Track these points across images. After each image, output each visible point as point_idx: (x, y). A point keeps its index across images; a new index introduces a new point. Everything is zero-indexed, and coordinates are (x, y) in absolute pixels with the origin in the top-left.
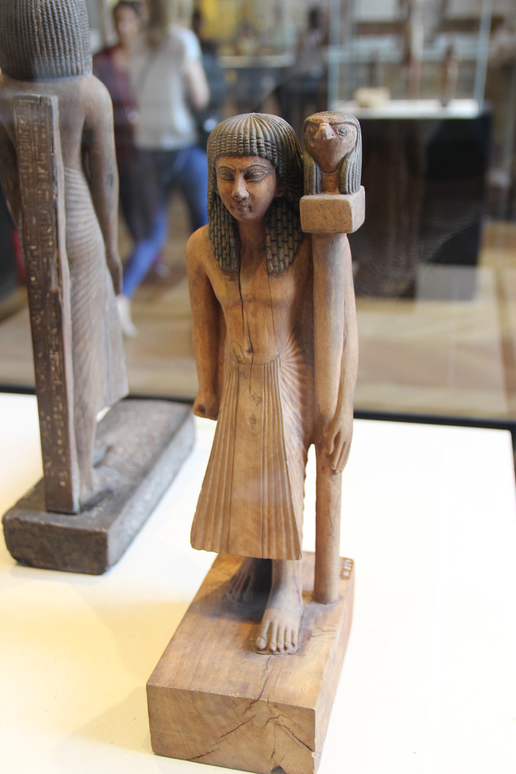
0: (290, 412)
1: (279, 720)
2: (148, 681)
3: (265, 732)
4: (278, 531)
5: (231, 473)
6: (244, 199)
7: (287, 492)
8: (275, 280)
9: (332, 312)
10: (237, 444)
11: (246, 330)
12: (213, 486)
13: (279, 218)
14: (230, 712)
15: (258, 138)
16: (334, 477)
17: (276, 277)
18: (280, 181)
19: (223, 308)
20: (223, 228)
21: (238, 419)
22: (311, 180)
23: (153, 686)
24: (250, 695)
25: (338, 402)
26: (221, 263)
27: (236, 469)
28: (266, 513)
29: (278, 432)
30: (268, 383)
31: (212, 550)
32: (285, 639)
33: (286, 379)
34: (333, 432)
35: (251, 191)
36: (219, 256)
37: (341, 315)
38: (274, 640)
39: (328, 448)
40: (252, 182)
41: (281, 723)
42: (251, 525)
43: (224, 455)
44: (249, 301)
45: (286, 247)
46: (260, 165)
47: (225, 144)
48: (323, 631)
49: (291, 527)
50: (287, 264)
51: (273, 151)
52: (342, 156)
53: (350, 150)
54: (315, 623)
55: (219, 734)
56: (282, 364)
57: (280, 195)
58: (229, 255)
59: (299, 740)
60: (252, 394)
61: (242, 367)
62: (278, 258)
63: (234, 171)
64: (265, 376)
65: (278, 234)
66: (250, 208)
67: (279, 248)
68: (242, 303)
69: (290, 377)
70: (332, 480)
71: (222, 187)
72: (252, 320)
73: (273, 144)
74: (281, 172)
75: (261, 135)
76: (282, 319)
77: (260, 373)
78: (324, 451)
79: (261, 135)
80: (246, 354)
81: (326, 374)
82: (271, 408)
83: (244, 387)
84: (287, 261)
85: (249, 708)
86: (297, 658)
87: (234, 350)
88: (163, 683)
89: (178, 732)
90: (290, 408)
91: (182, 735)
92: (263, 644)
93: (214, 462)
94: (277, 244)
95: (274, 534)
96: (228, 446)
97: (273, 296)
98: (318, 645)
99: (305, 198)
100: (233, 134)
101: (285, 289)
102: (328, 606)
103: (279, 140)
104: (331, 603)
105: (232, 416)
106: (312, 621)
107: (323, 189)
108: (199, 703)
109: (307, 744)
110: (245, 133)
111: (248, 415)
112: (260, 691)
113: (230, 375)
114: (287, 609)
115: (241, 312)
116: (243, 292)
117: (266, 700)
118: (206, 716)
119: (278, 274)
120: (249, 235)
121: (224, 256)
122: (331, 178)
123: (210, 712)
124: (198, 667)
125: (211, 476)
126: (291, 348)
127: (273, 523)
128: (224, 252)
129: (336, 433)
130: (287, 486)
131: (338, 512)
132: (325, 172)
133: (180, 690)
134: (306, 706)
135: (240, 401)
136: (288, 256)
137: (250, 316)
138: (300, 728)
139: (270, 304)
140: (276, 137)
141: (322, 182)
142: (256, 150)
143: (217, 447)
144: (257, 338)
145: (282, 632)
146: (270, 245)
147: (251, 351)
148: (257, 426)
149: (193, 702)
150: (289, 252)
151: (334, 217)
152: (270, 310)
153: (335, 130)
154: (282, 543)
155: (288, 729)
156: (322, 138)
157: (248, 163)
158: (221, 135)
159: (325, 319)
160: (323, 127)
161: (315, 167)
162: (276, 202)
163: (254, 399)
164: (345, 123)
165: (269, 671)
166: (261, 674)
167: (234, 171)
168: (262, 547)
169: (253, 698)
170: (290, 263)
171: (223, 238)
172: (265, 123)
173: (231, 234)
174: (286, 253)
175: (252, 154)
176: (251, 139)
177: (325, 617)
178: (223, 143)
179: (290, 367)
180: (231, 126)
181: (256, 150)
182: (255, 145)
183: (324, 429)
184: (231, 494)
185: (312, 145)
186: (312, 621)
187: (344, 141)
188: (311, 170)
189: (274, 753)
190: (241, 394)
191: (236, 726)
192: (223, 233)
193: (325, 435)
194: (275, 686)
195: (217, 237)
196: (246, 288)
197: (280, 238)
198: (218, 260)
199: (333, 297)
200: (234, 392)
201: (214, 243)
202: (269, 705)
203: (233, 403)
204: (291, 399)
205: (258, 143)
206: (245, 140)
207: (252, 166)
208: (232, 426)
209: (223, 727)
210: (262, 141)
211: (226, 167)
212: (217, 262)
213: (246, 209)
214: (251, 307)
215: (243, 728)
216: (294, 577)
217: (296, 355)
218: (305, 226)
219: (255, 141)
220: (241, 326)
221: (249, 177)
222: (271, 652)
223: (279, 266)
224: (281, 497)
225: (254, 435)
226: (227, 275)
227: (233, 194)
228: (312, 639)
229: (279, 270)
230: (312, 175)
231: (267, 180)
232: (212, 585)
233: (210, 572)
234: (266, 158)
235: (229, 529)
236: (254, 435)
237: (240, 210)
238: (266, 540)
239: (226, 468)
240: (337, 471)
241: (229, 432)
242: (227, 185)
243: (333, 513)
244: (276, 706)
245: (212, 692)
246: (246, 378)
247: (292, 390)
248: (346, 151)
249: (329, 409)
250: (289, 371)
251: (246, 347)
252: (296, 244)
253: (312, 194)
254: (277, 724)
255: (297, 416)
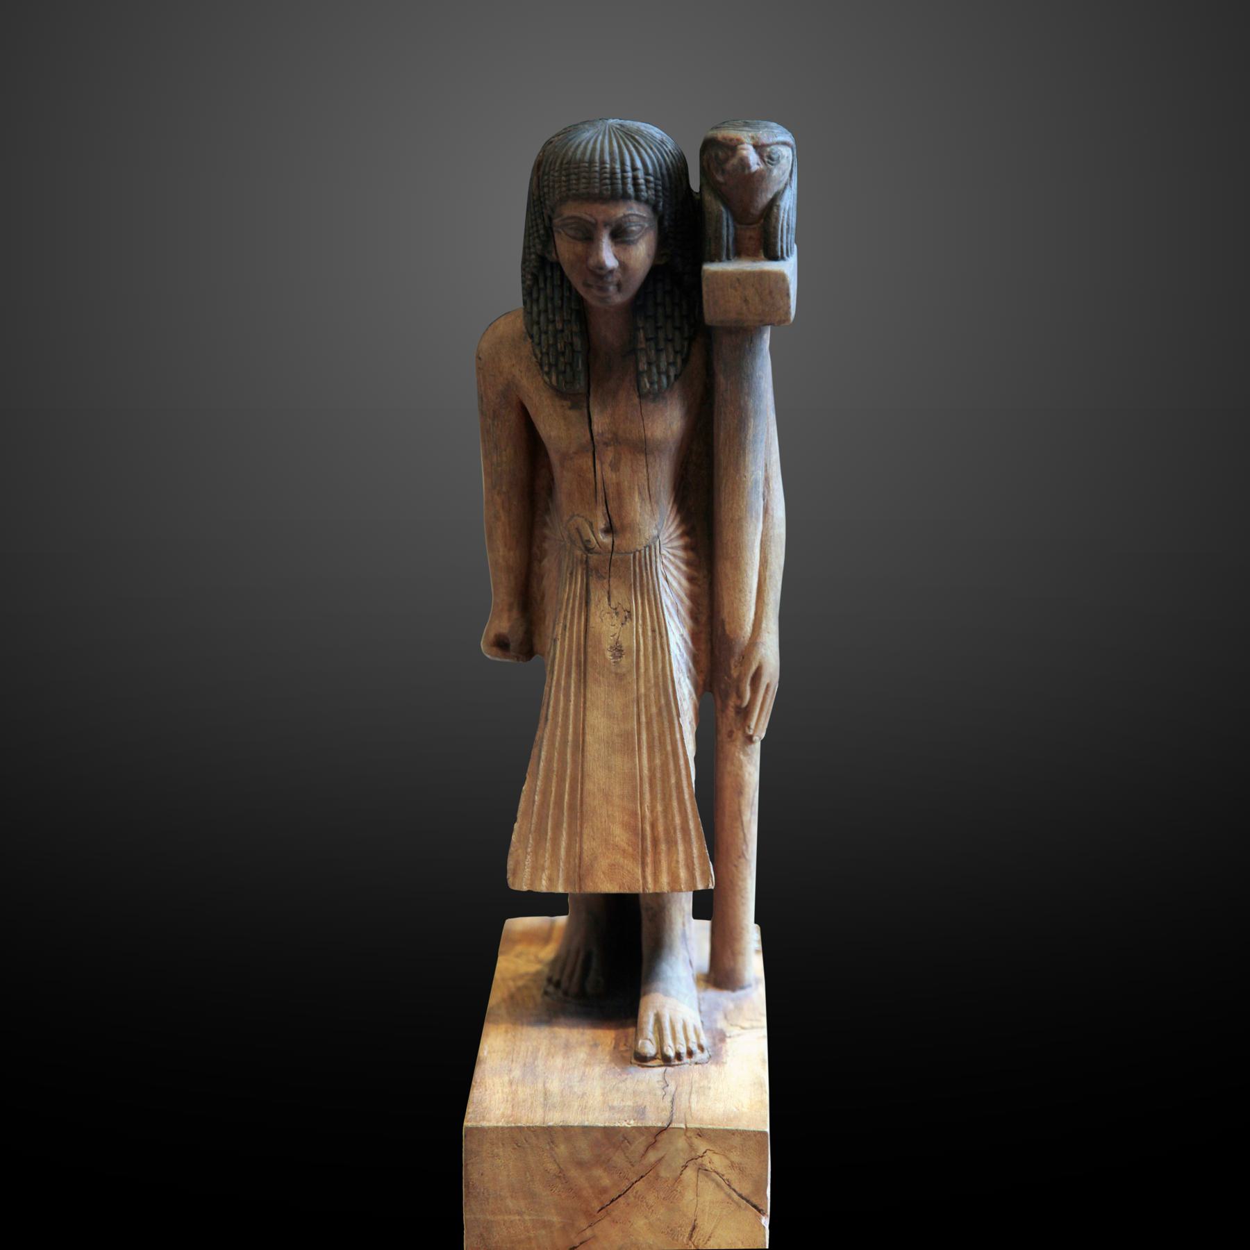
0: (677, 635)
1: (706, 1160)
3: (679, 1188)
4: (671, 843)
6: (611, 271)
8: (651, 406)
9: (749, 458)
10: (589, 695)
11: (600, 495)
13: (659, 300)
14: (619, 1159)
15: (634, 169)
17: (654, 400)
18: (663, 242)
19: (554, 458)
20: (557, 318)
21: (589, 650)
22: (718, 238)
23: (477, 1128)
24: (654, 1120)
25: (756, 614)
26: (554, 378)
27: (589, 738)
28: (648, 813)
29: (664, 668)
30: (642, 586)
32: (687, 1039)
33: (669, 578)
34: (750, 664)
35: (622, 258)
36: (550, 365)
37: (761, 463)
38: (669, 1040)
39: (740, 696)
40: (624, 242)
41: (709, 1166)
42: (620, 835)
43: (566, 716)
44: (606, 444)
45: (670, 350)
46: (636, 214)
47: (578, 179)
48: (743, 1028)
50: (672, 378)
51: (656, 191)
52: (770, 196)
53: (782, 186)
54: (726, 1017)
55: (596, 1205)
56: (664, 552)
57: (662, 262)
58: (571, 364)
59: (740, 1196)
60: (613, 605)
61: (594, 558)
62: (658, 367)
63: (595, 225)
64: (632, 571)
65: (657, 328)
66: (619, 286)
67: (658, 351)
68: (593, 448)
69: (675, 572)
70: (746, 754)
71: (565, 249)
72: (610, 476)
73: (656, 179)
74: (666, 223)
75: (639, 164)
76: (662, 473)
79: (639, 164)
80: (601, 536)
81: (738, 566)
82: (649, 628)
83: (598, 595)
84: (672, 374)
85: (652, 1146)
86: (712, 1069)
87: (578, 530)
89: (520, 1213)
90: (677, 628)
91: (527, 1218)
92: (650, 1049)
94: (657, 344)
95: (663, 847)
96: (572, 698)
97: (649, 434)
99: (710, 268)
100: (591, 162)
101: (668, 422)
102: (739, 993)
103: (665, 172)
104: (742, 988)
105: (578, 644)
106: (719, 1016)
107: (739, 252)
108: (562, 1149)
109: (753, 1200)
110: (613, 160)
111: (607, 643)
112: (668, 1114)
113: (571, 574)
115: (590, 463)
116: (595, 428)
117: (683, 1126)
118: (573, 1173)
119: (657, 396)
120: (608, 332)
121: (562, 367)
122: (749, 233)
123: (580, 1164)
124: (546, 1094)
126: (676, 523)
127: (661, 828)
128: (562, 359)
129: (754, 668)
132: (740, 223)
133: (529, 1128)
134: (752, 1128)
135: (592, 620)
136: (674, 364)
137: (607, 467)
138: (742, 1170)
139: (643, 448)
140: (660, 166)
141: (736, 240)
142: (631, 190)
144: (621, 506)
145: (679, 1028)
146: (643, 346)
147: (610, 530)
148: (624, 661)
149: (552, 1149)
150: (675, 358)
151: (761, 300)
152: (643, 457)
153: (761, 157)
154: (677, 862)
155: (721, 1176)
156: (743, 169)
157: (621, 211)
158: (569, 163)
159: (737, 470)
160: (745, 152)
161: (725, 216)
162: (655, 272)
163: (617, 614)
164: (777, 143)
165: (672, 1088)
166: (660, 1093)
167: (595, 225)
168: (644, 871)
169: (660, 1125)
170: (676, 377)
171: (559, 335)
172: (642, 142)
173: (575, 328)
174: (671, 360)
175: (625, 197)
176: (624, 171)
177: (739, 1008)
178: (573, 177)
179: (674, 555)
180: (585, 148)
181: (631, 190)
182: (630, 180)
183: (732, 663)
184: (582, 784)
185: (720, 178)
186: (719, 1016)
187: (775, 172)
188: (719, 220)
189: (694, 1228)
190: (593, 608)
191: (628, 1184)
192: (559, 326)
193: (735, 674)
194: (690, 1107)
195: (546, 333)
196: (601, 422)
197: (661, 335)
198: (548, 374)
199: (751, 432)
200: (580, 604)
202: (689, 1134)
203: (579, 623)
204: (678, 611)
205: (635, 178)
206: (613, 173)
207: (625, 216)
208: (578, 665)
209: (604, 1191)
210: (641, 174)
211: (580, 219)
212: (546, 378)
213: (612, 288)
214: (609, 455)
215: (639, 1186)
216: (684, 935)
217: (682, 536)
218: (712, 314)
219: (630, 174)
220: (592, 487)
221: (620, 235)
222: (666, 1061)
223: (659, 381)
224: (673, 781)
225: (620, 677)
226: (565, 399)
227: (592, 262)
228: (728, 1040)
229: (660, 387)
230: (721, 228)
231: (646, 238)
234: (647, 202)
235: (581, 847)
236: (620, 677)
237: (603, 289)
238: (649, 860)
239: (570, 738)
241: (573, 675)
242: (579, 248)
244: (700, 1133)
245: (586, 1124)
246: (601, 577)
247: (678, 596)
248: (776, 189)
249: (741, 629)
250: (673, 563)
251: (601, 524)
252: (686, 344)
253: (720, 261)
254: (702, 1169)
255: (686, 642)
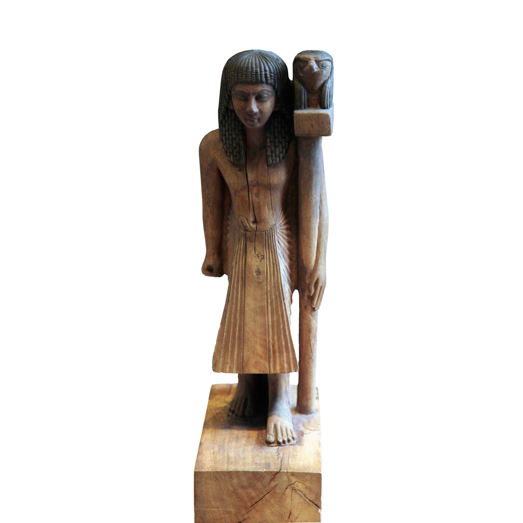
0: (283, 266)
1: (295, 486)
2: (195, 469)
3: (284, 497)
4: (281, 353)
5: (243, 312)
6: (256, 114)
7: (286, 323)
8: (272, 170)
9: (313, 191)
10: (246, 291)
11: (251, 207)
12: (230, 322)
13: (276, 125)
14: (259, 485)
15: (265, 71)
16: (314, 313)
17: (274, 167)
18: (277, 101)
19: (232, 192)
20: (233, 133)
21: (247, 272)
22: (301, 99)
23: (200, 472)
24: (274, 468)
25: (316, 257)
26: (232, 158)
27: (246, 309)
28: (271, 340)
29: (278, 279)
30: (268, 245)
31: (231, 371)
32: (287, 435)
33: (280, 242)
35: (260, 108)
36: (230, 153)
38: (280, 435)
39: (310, 291)
40: (261, 101)
41: (296, 488)
42: (259, 350)
43: (237, 299)
44: (254, 186)
45: (280, 146)
46: (266, 89)
47: (242, 75)
48: (311, 430)
49: (290, 349)
50: (281, 158)
51: (274, 80)
52: (322, 82)
53: (327, 78)
54: (304, 426)
55: (249, 504)
56: (278, 231)
57: (277, 110)
58: (239, 153)
59: (310, 500)
60: (257, 253)
61: (248, 234)
62: (275, 154)
63: (249, 94)
65: (275, 137)
66: (259, 120)
67: (275, 147)
68: (248, 187)
69: (282, 240)
70: (312, 315)
72: (255, 199)
73: (275, 75)
74: (279, 93)
75: (267, 69)
76: (277, 198)
77: (261, 237)
78: (306, 294)
79: (267, 69)
80: (251, 224)
81: (309, 237)
82: (272, 263)
83: (250, 249)
84: (281, 156)
85: (273, 479)
86: (298, 447)
87: (242, 222)
88: (208, 466)
89: (217, 508)
90: (283, 263)
91: (220, 509)
92: (272, 439)
93: (229, 306)
94: (275, 144)
95: (277, 354)
96: (239, 292)
97: (271, 182)
98: (309, 438)
99: (297, 112)
100: (247, 68)
101: (279, 177)
103: (278, 72)
104: (311, 413)
106: (301, 425)
107: (309, 106)
108: (235, 481)
109: (315, 502)
110: (256, 67)
111: (254, 269)
112: (280, 466)
113: (239, 240)
114: (283, 418)
115: (247, 194)
116: (249, 179)
117: (286, 471)
118: (240, 491)
119: (275, 166)
120: (254, 139)
121: (235, 154)
122: (313, 98)
123: (243, 487)
124: (229, 458)
125: (227, 315)
126: (283, 219)
127: (276, 347)
128: (235, 150)
129: (315, 280)
130: (285, 319)
131: (315, 340)
132: (310, 93)
133: (221, 472)
134: (315, 472)
135: (248, 259)
136: (282, 152)
137: (254, 196)
138: (310, 490)
139: (269, 188)
140: (276, 69)
141: (308, 100)
142: (264, 80)
143: (231, 294)
144: (260, 212)
145: (284, 430)
146: (269, 145)
147: (255, 222)
148: (261, 276)
149: (231, 481)
150: (282, 150)
151: (319, 125)
152: (269, 191)
153: (319, 66)
154: (283, 361)
155: (302, 492)
156: (311, 71)
157: (260, 88)
158: (238, 68)
159: (309, 197)
160: (312, 64)
161: (303, 90)
162: (274, 114)
163: (258, 257)
164: (325, 60)
165: (281, 455)
166: (276, 457)
167: (249, 94)
168: (269, 365)
169: (276, 471)
170: (283, 158)
171: (234, 140)
172: (269, 59)
173: (241, 137)
174: (281, 151)
175: (262, 82)
176: (261, 72)
177: (309, 422)
178: (240, 74)
179: (282, 232)
180: (245, 62)
181: (264, 80)
182: (263, 75)
183: (306, 277)
184: (244, 328)
185: (301, 75)
186: (301, 425)
187: (324, 72)
188: (301, 92)
189: (290, 514)
190: (248, 255)
191: (263, 495)
192: (234, 136)
193: (307, 282)
194: (289, 463)
195: (229, 139)
196: (251, 177)
197: (277, 140)
198: (229, 156)
199: (314, 181)
200: (243, 253)
201: (226, 144)
202: (288, 474)
203: (242, 261)
204: (284, 255)
205: (266, 75)
206: (256, 72)
207: (262, 90)
208: (242, 278)
209: (253, 498)
210: (268, 73)
211: (243, 91)
212: (229, 158)
213: (256, 121)
214: (255, 190)
215: (268, 496)
216: (286, 391)
217: (285, 224)
218: (298, 131)
219: (264, 73)
220: (248, 204)
221: (259, 98)
222: (279, 444)
223: (276, 160)
224: (282, 327)
225: (260, 283)
226: (237, 167)
227: (248, 110)
228: (305, 435)
229: (276, 162)
230: (302, 95)
231: (270, 100)
232: (215, 410)
233: (209, 402)
234: (271, 84)
235: (243, 354)
236: (260, 283)
237: (252, 121)
238: (272, 360)
239: (239, 309)
240: (316, 309)
241: (240, 283)
242: (242, 104)
243: (312, 342)
244: (293, 474)
245: (245, 470)
246: (251, 241)
247: (284, 249)
248: (325, 79)
249: (310, 263)
250: (282, 236)
251: (252, 219)
252: (287, 144)
253: (301, 109)
254: (294, 489)
255: (287, 269)
